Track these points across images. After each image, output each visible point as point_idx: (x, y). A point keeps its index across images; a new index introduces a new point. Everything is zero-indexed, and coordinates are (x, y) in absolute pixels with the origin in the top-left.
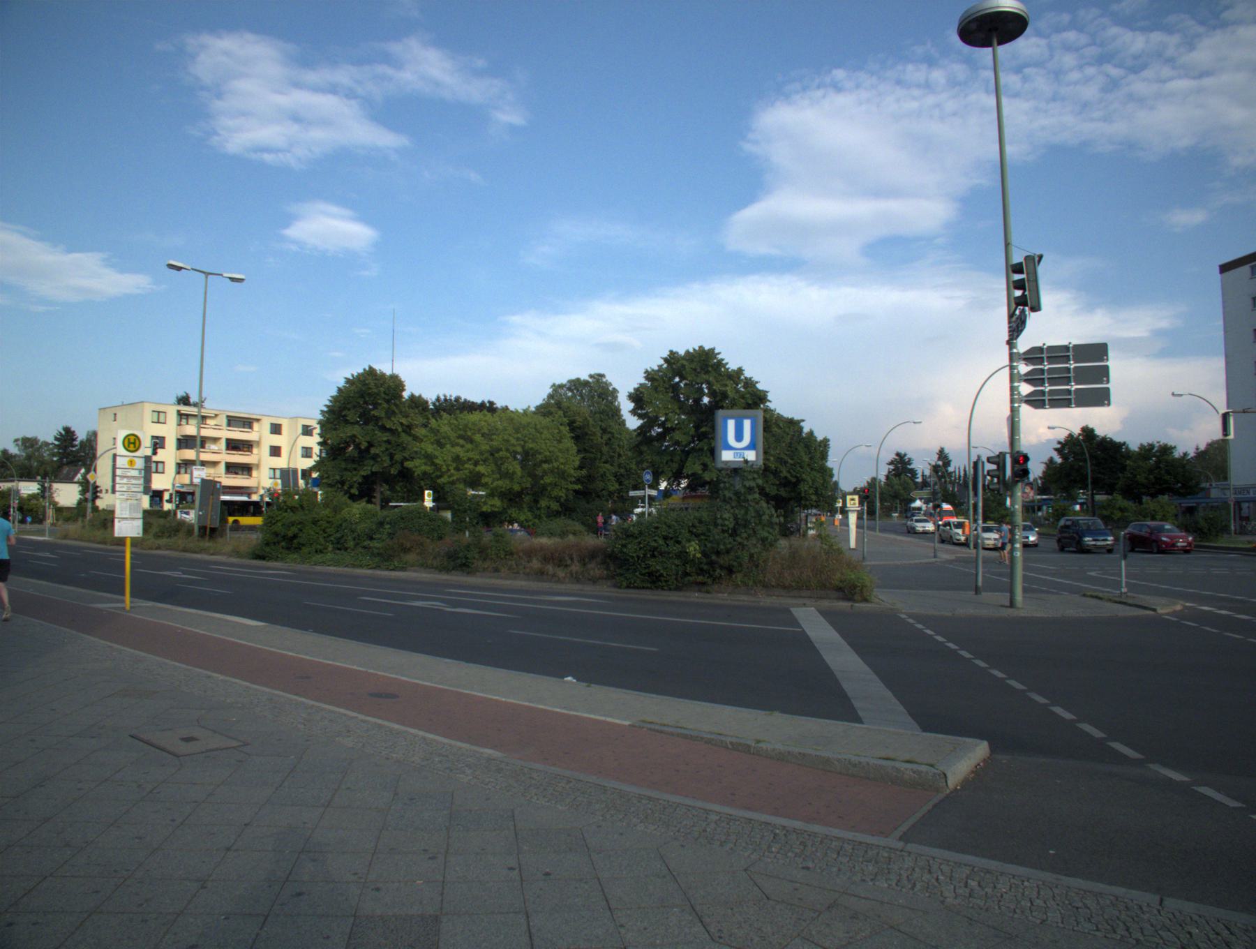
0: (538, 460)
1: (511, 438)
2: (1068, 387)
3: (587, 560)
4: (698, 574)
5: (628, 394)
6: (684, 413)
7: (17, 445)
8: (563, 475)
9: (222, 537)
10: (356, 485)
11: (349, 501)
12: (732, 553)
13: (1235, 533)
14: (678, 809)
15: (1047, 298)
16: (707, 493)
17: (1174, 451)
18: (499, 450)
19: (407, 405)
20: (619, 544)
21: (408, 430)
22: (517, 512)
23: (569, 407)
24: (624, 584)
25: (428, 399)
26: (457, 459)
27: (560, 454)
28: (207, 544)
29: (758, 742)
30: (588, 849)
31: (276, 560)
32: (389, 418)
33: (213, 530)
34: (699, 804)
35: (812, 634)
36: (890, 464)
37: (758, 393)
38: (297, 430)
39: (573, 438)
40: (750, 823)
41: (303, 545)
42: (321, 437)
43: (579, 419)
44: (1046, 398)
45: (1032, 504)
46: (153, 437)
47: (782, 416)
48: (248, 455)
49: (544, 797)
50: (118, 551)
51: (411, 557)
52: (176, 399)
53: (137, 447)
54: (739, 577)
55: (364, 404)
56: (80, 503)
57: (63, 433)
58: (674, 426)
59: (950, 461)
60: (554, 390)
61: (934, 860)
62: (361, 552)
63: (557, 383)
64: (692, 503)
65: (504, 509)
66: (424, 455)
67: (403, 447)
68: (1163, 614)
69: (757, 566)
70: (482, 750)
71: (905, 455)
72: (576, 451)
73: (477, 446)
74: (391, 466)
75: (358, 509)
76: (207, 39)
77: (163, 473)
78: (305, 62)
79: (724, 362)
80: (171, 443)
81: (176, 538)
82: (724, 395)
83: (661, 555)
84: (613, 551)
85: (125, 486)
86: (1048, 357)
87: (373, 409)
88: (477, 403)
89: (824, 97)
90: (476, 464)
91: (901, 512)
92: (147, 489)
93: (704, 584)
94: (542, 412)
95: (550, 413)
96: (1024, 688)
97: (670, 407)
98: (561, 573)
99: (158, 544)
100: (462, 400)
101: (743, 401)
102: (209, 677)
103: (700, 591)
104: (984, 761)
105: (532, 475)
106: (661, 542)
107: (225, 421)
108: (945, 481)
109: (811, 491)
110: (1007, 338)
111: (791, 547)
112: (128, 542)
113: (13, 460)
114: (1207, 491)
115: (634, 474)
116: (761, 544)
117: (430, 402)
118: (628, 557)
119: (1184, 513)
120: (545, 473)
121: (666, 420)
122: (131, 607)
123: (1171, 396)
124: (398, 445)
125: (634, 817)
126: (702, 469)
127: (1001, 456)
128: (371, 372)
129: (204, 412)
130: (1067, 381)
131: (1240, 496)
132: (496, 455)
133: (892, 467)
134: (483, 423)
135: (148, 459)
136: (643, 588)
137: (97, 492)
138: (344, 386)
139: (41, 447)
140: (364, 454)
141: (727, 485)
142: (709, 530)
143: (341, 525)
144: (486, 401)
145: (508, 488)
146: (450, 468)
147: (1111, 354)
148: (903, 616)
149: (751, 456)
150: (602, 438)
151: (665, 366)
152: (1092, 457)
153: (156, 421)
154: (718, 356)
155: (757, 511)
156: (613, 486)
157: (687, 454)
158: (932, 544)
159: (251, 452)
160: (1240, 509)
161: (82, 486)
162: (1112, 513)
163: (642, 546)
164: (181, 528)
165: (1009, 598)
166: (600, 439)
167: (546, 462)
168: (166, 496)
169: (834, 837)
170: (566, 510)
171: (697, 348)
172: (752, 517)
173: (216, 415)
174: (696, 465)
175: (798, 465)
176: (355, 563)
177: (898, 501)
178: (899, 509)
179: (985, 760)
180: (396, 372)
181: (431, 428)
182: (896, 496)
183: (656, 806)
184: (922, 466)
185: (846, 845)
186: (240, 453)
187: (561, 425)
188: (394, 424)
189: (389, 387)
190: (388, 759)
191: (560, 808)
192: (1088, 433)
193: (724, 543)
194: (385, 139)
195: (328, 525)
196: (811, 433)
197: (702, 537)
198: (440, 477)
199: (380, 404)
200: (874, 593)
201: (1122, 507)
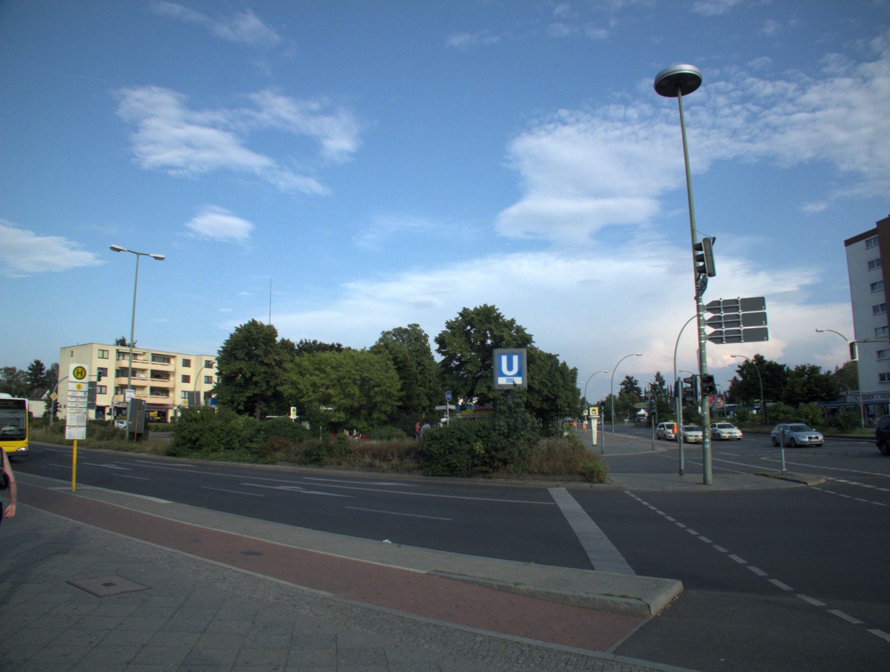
0: (371, 385)
1: (352, 370)
2: (739, 328)
3: (403, 456)
4: (483, 465)
5: (434, 338)
6: (474, 351)
8: (389, 395)
9: (145, 439)
10: (243, 403)
11: (236, 415)
12: (507, 450)
13: (865, 427)
14: (455, 633)
15: (720, 265)
16: (492, 407)
17: (820, 370)
18: (343, 378)
19: (279, 347)
20: (426, 445)
21: (280, 364)
22: (357, 422)
23: (393, 348)
24: (430, 473)
25: (295, 342)
26: (314, 385)
27: (387, 381)
29: (517, 584)
30: (387, 662)
31: (183, 457)
32: (266, 356)
33: (139, 435)
34: (470, 629)
35: (562, 506)
36: (622, 384)
37: (526, 336)
38: (201, 363)
39: (396, 369)
40: (505, 642)
41: (203, 446)
42: (219, 369)
43: (400, 356)
44: (724, 336)
45: (722, 410)
46: (99, 368)
47: (543, 352)
48: (167, 382)
49: (360, 625)
50: (66, 449)
51: (279, 455)
52: (115, 341)
53: (83, 376)
54: (511, 467)
55: (248, 346)
56: (45, 414)
57: (35, 364)
58: (467, 360)
59: (664, 381)
60: (383, 336)
61: (635, 667)
62: (244, 451)
63: (386, 330)
64: (478, 415)
65: (347, 419)
66: (290, 382)
68: (812, 486)
69: (524, 459)
70: (318, 592)
71: (632, 378)
72: (398, 378)
73: (328, 376)
74: (268, 389)
75: (242, 420)
77: (105, 394)
79: (501, 315)
80: (112, 373)
81: (112, 440)
82: (502, 338)
83: (456, 451)
84: (422, 449)
85: (74, 403)
86: (724, 308)
87: (255, 350)
88: (328, 345)
90: (328, 388)
91: (630, 418)
92: (91, 404)
93: (487, 472)
94: (374, 351)
95: (380, 352)
96: (710, 541)
97: (464, 347)
98: (385, 466)
99: (100, 445)
100: (318, 343)
101: (515, 342)
102: (128, 540)
103: (484, 477)
104: (679, 595)
105: (367, 395)
106: (456, 442)
107: (150, 357)
108: (661, 396)
110: (694, 295)
111: (548, 445)
112: (75, 443)
114: (844, 397)
115: (440, 394)
116: (527, 443)
117: (296, 344)
118: (433, 454)
119: (829, 414)
120: (376, 393)
121: (462, 356)
122: (76, 490)
123: (815, 332)
124: (272, 375)
125: (423, 639)
126: (488, 390)
127: (694, 378)
128: (253, 323)
129: (134, 351)
131: (867, 400)
132: (342, 381)
133: (623, 387)
134: (333, 359)
135: (92, 384)
136: (444, 476)
137: (57, 407)
138: (234, 333)
139: (18, 375)
140: (248, 381)
141: (502, 402)
142: (490, 434)
143: (230, 432)
144: (335, 343)
146: (309, 391)
147: (767, 303)
148: (627, 492)
149: (519, 381)
150: (417, 369)
151: (460, 318)
152: (762, 376)
154: (497, 311)
155: (523, 420)
156: (425, 402)
157: (476, 379)
158: (651, 441)
159: (169, 379)
160: (868, 410)
161: (47, 403)
162: (778, 415)
163: (442, 445)
164: (116, 433)
165: (702, 477)
166: (415, 370)
167: (378, 386)
168: (107, 410)
169: (565, 652)
170: (392, 420)
171: (482, 306)
172: (520, 424)
173: (144, 353)
174: (483, 388)
175: (556, 387)
176: (240, 459)
177: (628, 411)
179: (679, 594)
180: (272, 323)
181: (296, 363)
182: (626, 407)
183: (439, 631)
184: (644, 386)
185: (572, 658)
186: (161, 380)
187: (388, 360)
188: (270, 360)
189: (266, 334)
190: (250, 598)
191: (370, 633)
192: (759, 359)
193: (501, 442)
195: (221, 432)
196: (564, 364)
197: (485, 439)
198: (302, 397)
199: (260, 346)
200: (607, 477)
201: (785, 410)
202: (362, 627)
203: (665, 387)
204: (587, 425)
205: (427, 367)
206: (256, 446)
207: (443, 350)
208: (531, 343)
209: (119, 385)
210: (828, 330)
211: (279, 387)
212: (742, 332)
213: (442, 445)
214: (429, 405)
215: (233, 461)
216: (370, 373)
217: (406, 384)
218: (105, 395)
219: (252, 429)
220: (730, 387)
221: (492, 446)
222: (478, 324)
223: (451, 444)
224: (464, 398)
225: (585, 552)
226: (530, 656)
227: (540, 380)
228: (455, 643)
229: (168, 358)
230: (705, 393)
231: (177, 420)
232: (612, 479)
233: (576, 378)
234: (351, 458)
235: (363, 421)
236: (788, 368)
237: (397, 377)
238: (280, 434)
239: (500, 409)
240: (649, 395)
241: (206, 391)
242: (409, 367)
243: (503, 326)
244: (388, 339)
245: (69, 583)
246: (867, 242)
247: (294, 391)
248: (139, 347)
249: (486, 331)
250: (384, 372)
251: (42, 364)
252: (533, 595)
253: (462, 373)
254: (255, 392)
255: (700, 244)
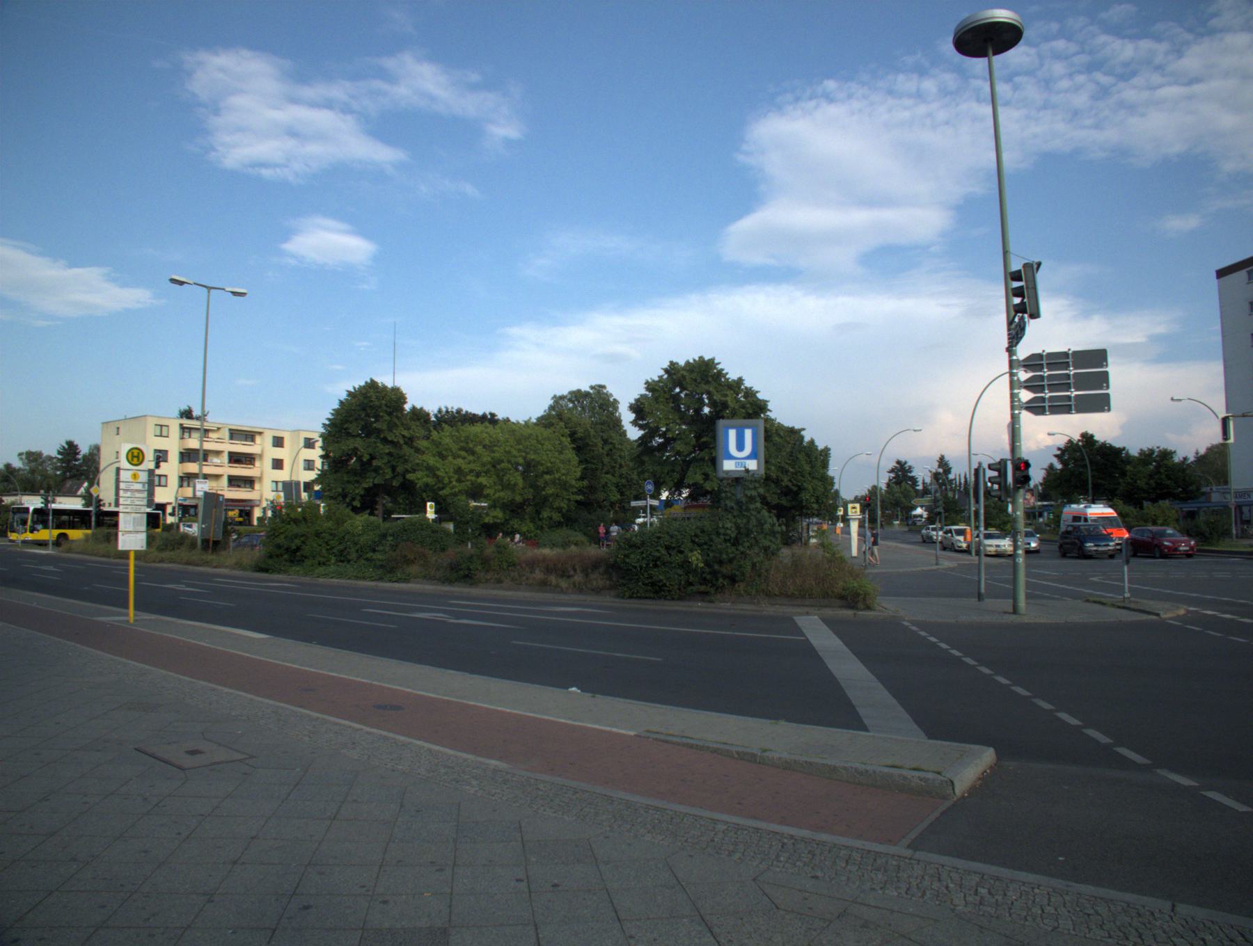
6: (685, 423)
7: (21, 459)
8: (564, 486)
9: (225, 549)
10: (358, 498)
11: (352, 514)
12: (735, 562)
16: (709, 503)
18: (502, 461)
21: (410, 443)
22: (520, 523)
23: (570, 419)
25: (430, 412)
26: (459, 471)
28: (210, 557)
29: (765, 751)
31: (279, 573)
32: (391, 431)
33: (216, 543)
34: (707, 814)
37: (758, 402)
39: (574, 448)
41: (306, 557)
43: (580, 430)
44: (1047, 404)
45: (1033, 510)
51: (414, 569)
54: (741, 587)
57: (66, 447)
58: (675, 437)
62: (364, 564)
63: (559, 394)
64: (694, 513)
67: (405, 459)
68: (1165, 619)
69: (760, 576)
71: (906, 463)
72: (578, 461)
73: (478, 458)
74: (393, 478)
76: (203, 56)
77: (166, 486)
78: (301, 78)
79: (724, 372)
80: (174, 457)
82: (725, 405)
84: (616, 561)
85: (129, 499)
87: (375, 422)
88: (478, 415)
89: (816, 107)
90: (478, 475)
91: (902, 520)
93: (706, 593)
94: (543, 424)
95: (551, 425)
97: (670, 417)
98: (564, 584)
100: (464, 412)
101: (744, 411)
103: (703, 601)
105: (534, 486)
106: (663, 551)
107: (227, 435)
108: (946, 489)
109: (813, 500)
113: (16, 474)
114: (1207, 495)
115: (635, 484)
121: (668, 430)
122: (136, 621)
128: (372, 385)
129: (207, 426)
130: (1067, 387)
131: (1240, 500)
132: (498, 467)
133: (892, 475)
134: (485, 435)
135: (151, 472)
136: (646, 598)
137: (101, 505)
138: (346, 399)
139: (44, 462)
140: (366, 466)
141: (729, 494)
142: (711, 540)
143: (343, 537)
144: (487, 413)
145: (510, 499)
146: (452, 480)
148: (906, 623)
149: (752, 465)
151: (666, 376)
152: (1091, 462)
153: (159, 434)
154: (717, 366)
155: (758, 521)
157: (688, 464)
158: (934, 552)
159: (254, 465)
160: (1242, 513)
161: (85, 500)
163: (644, 556)
165: (1012, 603)
166: (601, 450)
168: (169, 509)
169: (843, 846)
170: (568, 521)
171: (697, 359)
172: (754, 526)
173: (219, 429)
174: (697, 475)
175: (799, 474)
176: (359, 575)
177: (899, 509)
178: (900, 517)
180: (398, 384)
181: (433, 440)
182: (897, 504)
183: (663, 816)
184: (923, 474)
185: (854, 854)
187: (563, 436)
190: (393, 771)
192: (1088, 438)
194: (383, 154)
196: (812, 442)
197: (705, 547)
198: (443, 488)
199: (382, 417)
202: (554, 810)
203: (951, 476)
204: (842, 528)
205: (617, 446)
206: (380, 557)
207: (641, 422)
208: (766, 412)
209: (184, 474)
210: (1189, 399)
211: (410, 475)
212: (1073, 399)
213: (644, 556)
214: (619, 500)
215: (349, 578)
216: (538, 454)
217: (587, 469)
218: (165, 488)
219: (375, 534)
220: (1044, 479)
221: (714, 557)
222: (691, 384)
223: (657, 554)
224: (670, 489)
225: (853, 707)
226: (795, 852)
227: (778, 464)
228: (688, 833)
229: (252, 435)
230: (1018, 486)
231: (266, 522)
232: (884, 605)
233: (828, 461)
234: (516, 574)
235: (528, 521)
236: (1127, 453)
237: (575, 460)
238: (414, 539)
239: (726, 505)
240: (933, 487)
241: (307, 480)
242: (592, 446)
243: (726, 388)
244: (562, 406)
245: (139, 751)
246: (1249, 273)
247: (432, 480)
248: (212, 420)
249: (702, 394)
250: (557, 453)
251: (77, 446)
252: (787, 766)
253: (668, 454)
254: (376, 482)
255: (1019, 271)
